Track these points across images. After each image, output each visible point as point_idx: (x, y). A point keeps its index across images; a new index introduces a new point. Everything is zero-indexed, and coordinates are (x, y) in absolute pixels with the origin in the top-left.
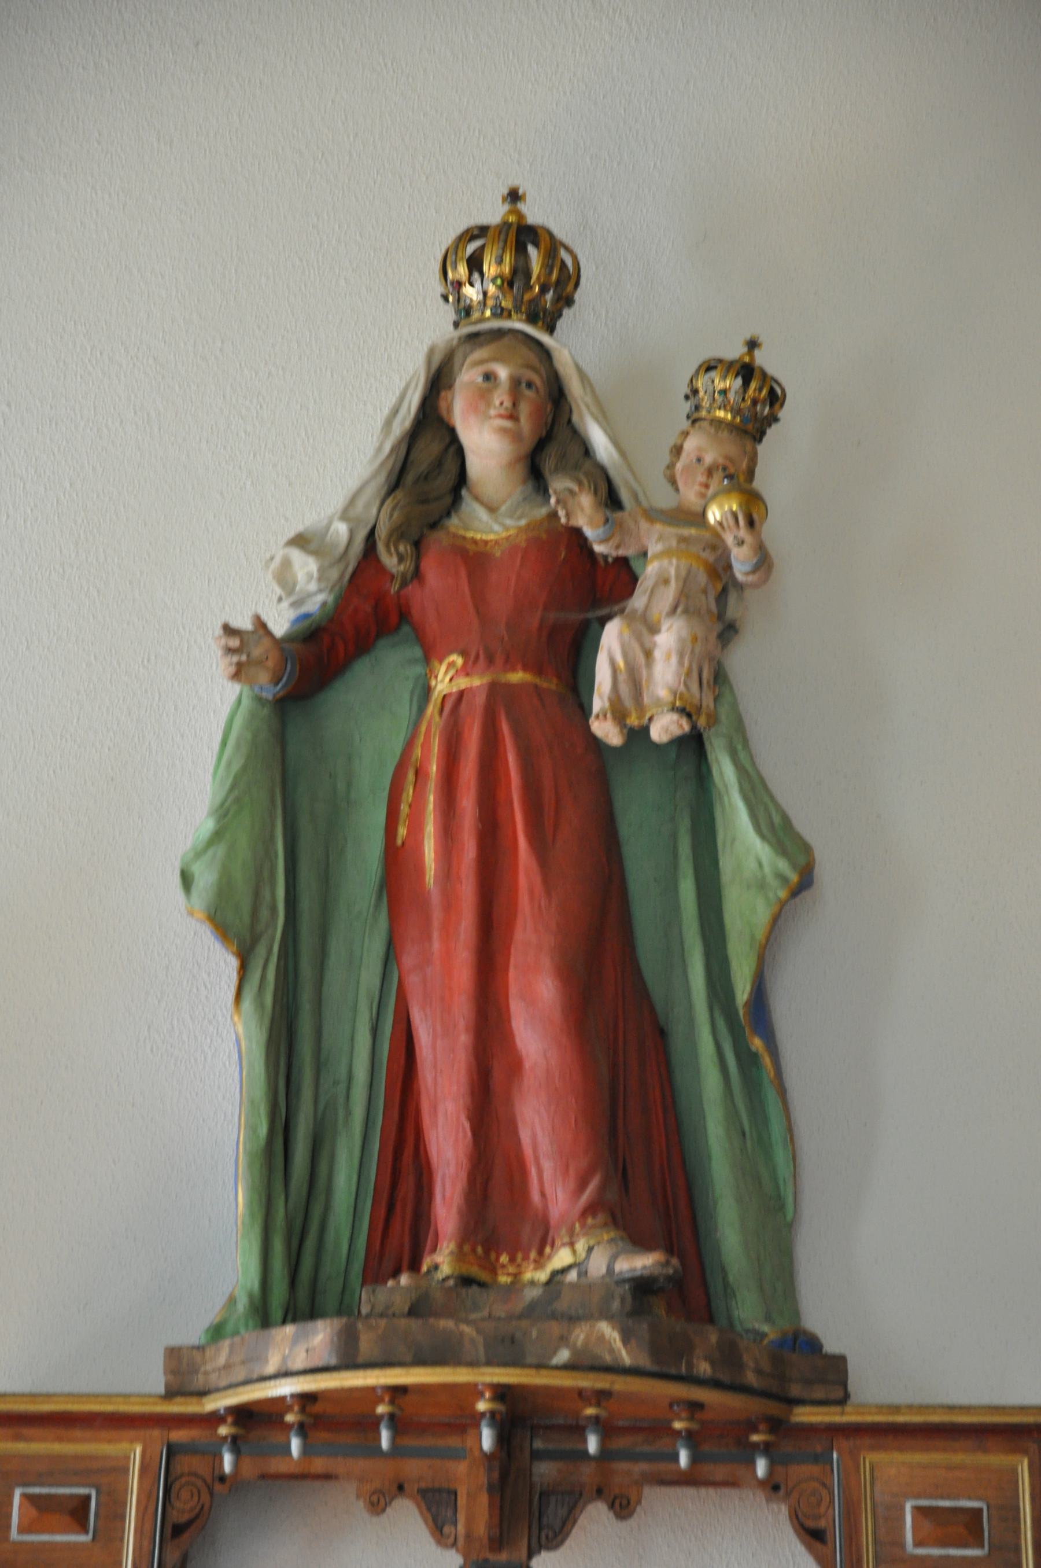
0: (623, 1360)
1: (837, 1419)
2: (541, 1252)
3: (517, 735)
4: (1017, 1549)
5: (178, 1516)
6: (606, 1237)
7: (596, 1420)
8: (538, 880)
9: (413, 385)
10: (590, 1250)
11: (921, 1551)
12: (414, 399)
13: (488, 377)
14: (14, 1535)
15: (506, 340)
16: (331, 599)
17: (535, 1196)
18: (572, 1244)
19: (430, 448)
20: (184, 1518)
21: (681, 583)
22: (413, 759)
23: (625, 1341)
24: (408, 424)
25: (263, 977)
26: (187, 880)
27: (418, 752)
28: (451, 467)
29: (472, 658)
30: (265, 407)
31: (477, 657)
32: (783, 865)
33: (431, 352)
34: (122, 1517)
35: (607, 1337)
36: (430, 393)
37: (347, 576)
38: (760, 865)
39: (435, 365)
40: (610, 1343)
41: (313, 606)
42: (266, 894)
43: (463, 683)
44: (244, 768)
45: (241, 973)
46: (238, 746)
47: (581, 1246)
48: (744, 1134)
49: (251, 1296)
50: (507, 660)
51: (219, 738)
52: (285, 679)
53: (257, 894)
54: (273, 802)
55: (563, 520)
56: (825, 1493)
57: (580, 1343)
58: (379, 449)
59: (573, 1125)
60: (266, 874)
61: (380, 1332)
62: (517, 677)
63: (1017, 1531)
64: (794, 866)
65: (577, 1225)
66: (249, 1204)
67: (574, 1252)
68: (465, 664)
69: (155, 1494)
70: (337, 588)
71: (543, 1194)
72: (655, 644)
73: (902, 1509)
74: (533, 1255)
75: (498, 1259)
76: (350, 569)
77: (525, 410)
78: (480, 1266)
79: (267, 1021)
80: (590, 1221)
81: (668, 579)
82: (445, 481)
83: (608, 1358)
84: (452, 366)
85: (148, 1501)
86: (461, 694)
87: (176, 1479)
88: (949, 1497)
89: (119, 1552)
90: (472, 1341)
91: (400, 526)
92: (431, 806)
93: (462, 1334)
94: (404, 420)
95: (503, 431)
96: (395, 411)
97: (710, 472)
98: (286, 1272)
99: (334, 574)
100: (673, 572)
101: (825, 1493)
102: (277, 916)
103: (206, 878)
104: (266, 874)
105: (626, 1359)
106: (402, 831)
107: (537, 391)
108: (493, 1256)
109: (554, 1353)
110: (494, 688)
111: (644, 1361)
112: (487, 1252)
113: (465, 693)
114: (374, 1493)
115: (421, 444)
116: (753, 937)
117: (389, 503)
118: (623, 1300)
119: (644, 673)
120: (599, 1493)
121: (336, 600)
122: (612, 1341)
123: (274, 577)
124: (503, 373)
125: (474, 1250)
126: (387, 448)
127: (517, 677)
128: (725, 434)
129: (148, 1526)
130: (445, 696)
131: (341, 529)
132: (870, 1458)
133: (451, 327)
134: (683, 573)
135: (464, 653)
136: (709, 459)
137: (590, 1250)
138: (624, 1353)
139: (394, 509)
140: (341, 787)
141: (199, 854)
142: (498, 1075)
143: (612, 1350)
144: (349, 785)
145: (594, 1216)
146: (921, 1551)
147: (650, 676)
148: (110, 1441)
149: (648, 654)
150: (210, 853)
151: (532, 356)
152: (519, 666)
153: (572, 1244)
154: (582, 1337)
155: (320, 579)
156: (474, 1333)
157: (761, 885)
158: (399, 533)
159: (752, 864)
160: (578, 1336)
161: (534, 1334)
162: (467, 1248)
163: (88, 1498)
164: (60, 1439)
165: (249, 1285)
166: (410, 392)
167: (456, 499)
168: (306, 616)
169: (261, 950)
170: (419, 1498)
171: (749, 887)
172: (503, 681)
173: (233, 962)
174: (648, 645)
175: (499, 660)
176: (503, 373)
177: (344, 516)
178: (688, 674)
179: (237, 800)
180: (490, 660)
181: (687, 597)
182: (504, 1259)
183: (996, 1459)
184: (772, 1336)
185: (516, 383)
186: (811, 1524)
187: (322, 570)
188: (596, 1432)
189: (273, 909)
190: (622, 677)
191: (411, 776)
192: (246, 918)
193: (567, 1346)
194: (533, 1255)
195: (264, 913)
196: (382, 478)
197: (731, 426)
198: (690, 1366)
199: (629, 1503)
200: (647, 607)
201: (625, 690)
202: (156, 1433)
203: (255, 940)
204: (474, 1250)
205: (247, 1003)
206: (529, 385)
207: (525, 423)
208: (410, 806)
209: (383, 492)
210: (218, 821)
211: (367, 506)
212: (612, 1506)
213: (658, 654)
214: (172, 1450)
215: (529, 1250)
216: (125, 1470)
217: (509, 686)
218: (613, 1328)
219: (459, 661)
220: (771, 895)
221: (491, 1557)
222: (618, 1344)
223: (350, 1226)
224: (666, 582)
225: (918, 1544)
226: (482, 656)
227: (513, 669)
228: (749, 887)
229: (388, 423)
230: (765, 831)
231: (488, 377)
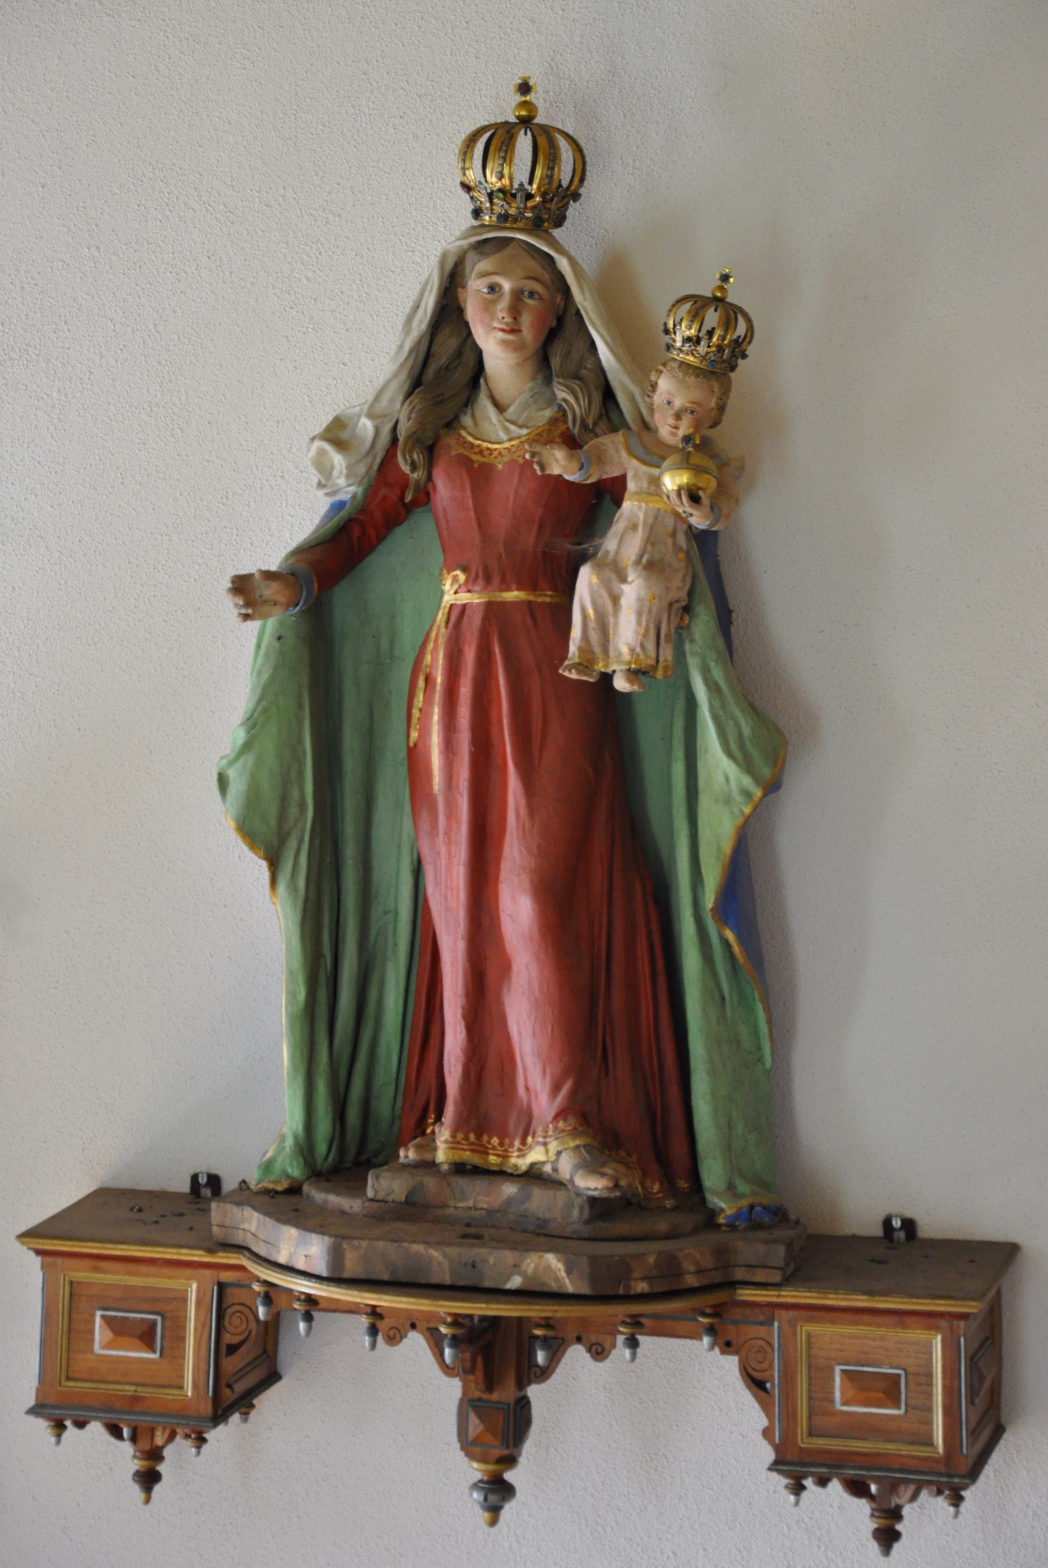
0: (566, 1287)
1: (775, 1300)
2: (524, 1142)
3: (507, 660)
4: (929, 1410)
5: (228, 1339)
6: (572, 1144)
7: (545, 1339)
8: (523, 803)
9: (429, 288)
10: (559, 1153)
11: (846, 1408)
12: (430, 302)
13: (493, 288)
14: (97, 1349)
15: (509, 250)
16: (360, 490)
17: (521, 1090)
18: (545, 1144)
19: (448, 344)
20: (235, 1340)
21: (647, 531)
22: (424, 664)
23: (569, 1272)
24: (424, 326)
25: (296, 865)
26: (223, 781)
27: (428, 658)
28: (469, 358)
29: (473, 575)
30: (323, 253)
31: (477, 576)
32: (747, 782)
33: (444, 256)
34: (183, 1339)
35: (553, 1267)
36: (450, 282)
37: (376, 467)
38: (727, 780)
39: (449, 265)
40: (555, 1273)
41: (345, 496)
42: (295, 794)
43: (464, 598)
44: (272, 679)
45: (272, 869)
46: (267, 654)
47: (554, 1146)
48: (723, 999)
49: (296, 1137)
50: (503, 580)
51: (254, 640)
52: (301, 604)
53: (284, 799)
54: (300, 706)
55: (539, 473)
56: (769, 1350)
57: (530, 1271)
58: (401, 347)
59: (549, 1032)
60: (294, 775)
61: (362, 1251)
62: (513, 595)
63: (930, 1395)
64: (757, 780)
65: (551, 1126)
66: (292, 1059)
67: (547, 1152)
68: (466, 581)
69: (208, 1324)
70: (365, 480)
71: (527, 1089)
72: (622, 593)
73: (833, 1370)
74: (517, 1143)
75: (489, 1142)
76: (378, 460)
77: (526, 320)
78: (473, 1151)
79: (300, 903)
80: (561, 1124)
81: (634, 524)
82: (462, 375)
83: (554, 1287)
84: (464, 269)
85: (203, 1330)
86: (464, 607)
87: (229, 1307)
88: (872, 1366)
89: (183, 1370)
90: (440, 1264)
91: (415, 433)
92: (436, 718)
93: (431, 1258)
94: (421, 321)
95: (505, 343)
96: (416, 307)
97: (678, 416)
98: (329, 1109)
99: (362, 469)
100: (641, 516)
101: (769, 1350)
102: (306, 811)
103: (238, 785)
104: (294, 775)
105: (570, 1288)
106: (414, 735)
107: (541, 298)
108: (485, 1138)
109: (508, 1279)
110: (491, 609)
111: (585, 1289)
112: (479, 1137)
113: (467, 607)
114: (392, 1328)
115: (440, 339)
116: (719, 849)
117: (407, 402)
118: (581, 1208)
119: (611, 620)
120: (579, 1340)
121: (366, 491)
122: (557, 1270)
123: (312, 464)
124: (507, 285)
125: (466, 1138)
126: (408, 345)
127: (513, 595)
128: (691, 380)
129: (204, 1349)
130: (452, 606)
131: (366, 426)
132: (805, 1329)
133: (469, 216)
134: (651, 520)
135: (465, 569)
136: (678, 403)
137: (559, 1153)
138: (567, 1281)
139: (411, 412)
140: (385, 644)
141: (231, 763)
142: (492, 973)
143: (557, 1280)
144: (392, 642)
145: (565, 1120)
146: (846, 1408)
147: (616, 624)
148: (170, 1278)
149: (615, 600)
150: (242, 760)
151: (534, 266)
152: (514, 587)
153: (545, 1144)
154: (532, 1265)
155: (348, 476)
156: (441, 1258)
157: (728, 800)
158: (416, 439)
159: (721, 779)
160: (529, 1264)
161: (492, 1261)
162: (460, 1136)
163: (154, 1324)
164: (130, 1273)
165: (295, 1128)
166: (426, 294)
167: (469, 402)
168: (341, 505)
169: (292, 843)
170: (427, 1334)
171: (716, 800)
172: (499, 600)
173: (264, 864)
174: (616, 591)
175: (496, 580)
176: (507, 285)
177: (370, 416)
178: (645, 635)
179: (265, 711)
180: (488, 579)
181: (653, 544)
182: (495, 1141)
183: (916, 1335)
184: (729, 1212)
185: (517, 296)
186: (756, 1375)
187: (349, 467)
188: (543, 1349)
189: (302, 805)
190: (592, 625)
191: (421, 683)
192: (273, 823)
193: (520, 1274)
194: (517, 1143)
195: (293, 811)
196: (403, 376)
197: (697, 371)
198: (628, 1287)
199: (603, 1350)
200: (617, 553)
201: (594, 637)
202: (207, 1273)
203: (282, 838)
204: (466, 1138)
205: (282, 888)
206: (532, 294)
207: (527, 332)
208: (420, 710)
209: (406, 388)
210: (248, 732)
211: (391, 401)
212: (589, 1351)
213: (624, 601)
214: (222, 1287)
215: (514, 1139)
216: (185, 1300)
217: (504, 605)
218: (559, 1260)
219: (462, 577)
220: (736, 810)
221: (485, 1396)
222: (563, 1274)
223: (399, 1037)
224: (635, 527)
225: (845, 1403)
226: (481, 574)
227: (509, 590)
228: (716, 800)
229: (409, 320)
230: (734, 747)
231: (493, 288)
